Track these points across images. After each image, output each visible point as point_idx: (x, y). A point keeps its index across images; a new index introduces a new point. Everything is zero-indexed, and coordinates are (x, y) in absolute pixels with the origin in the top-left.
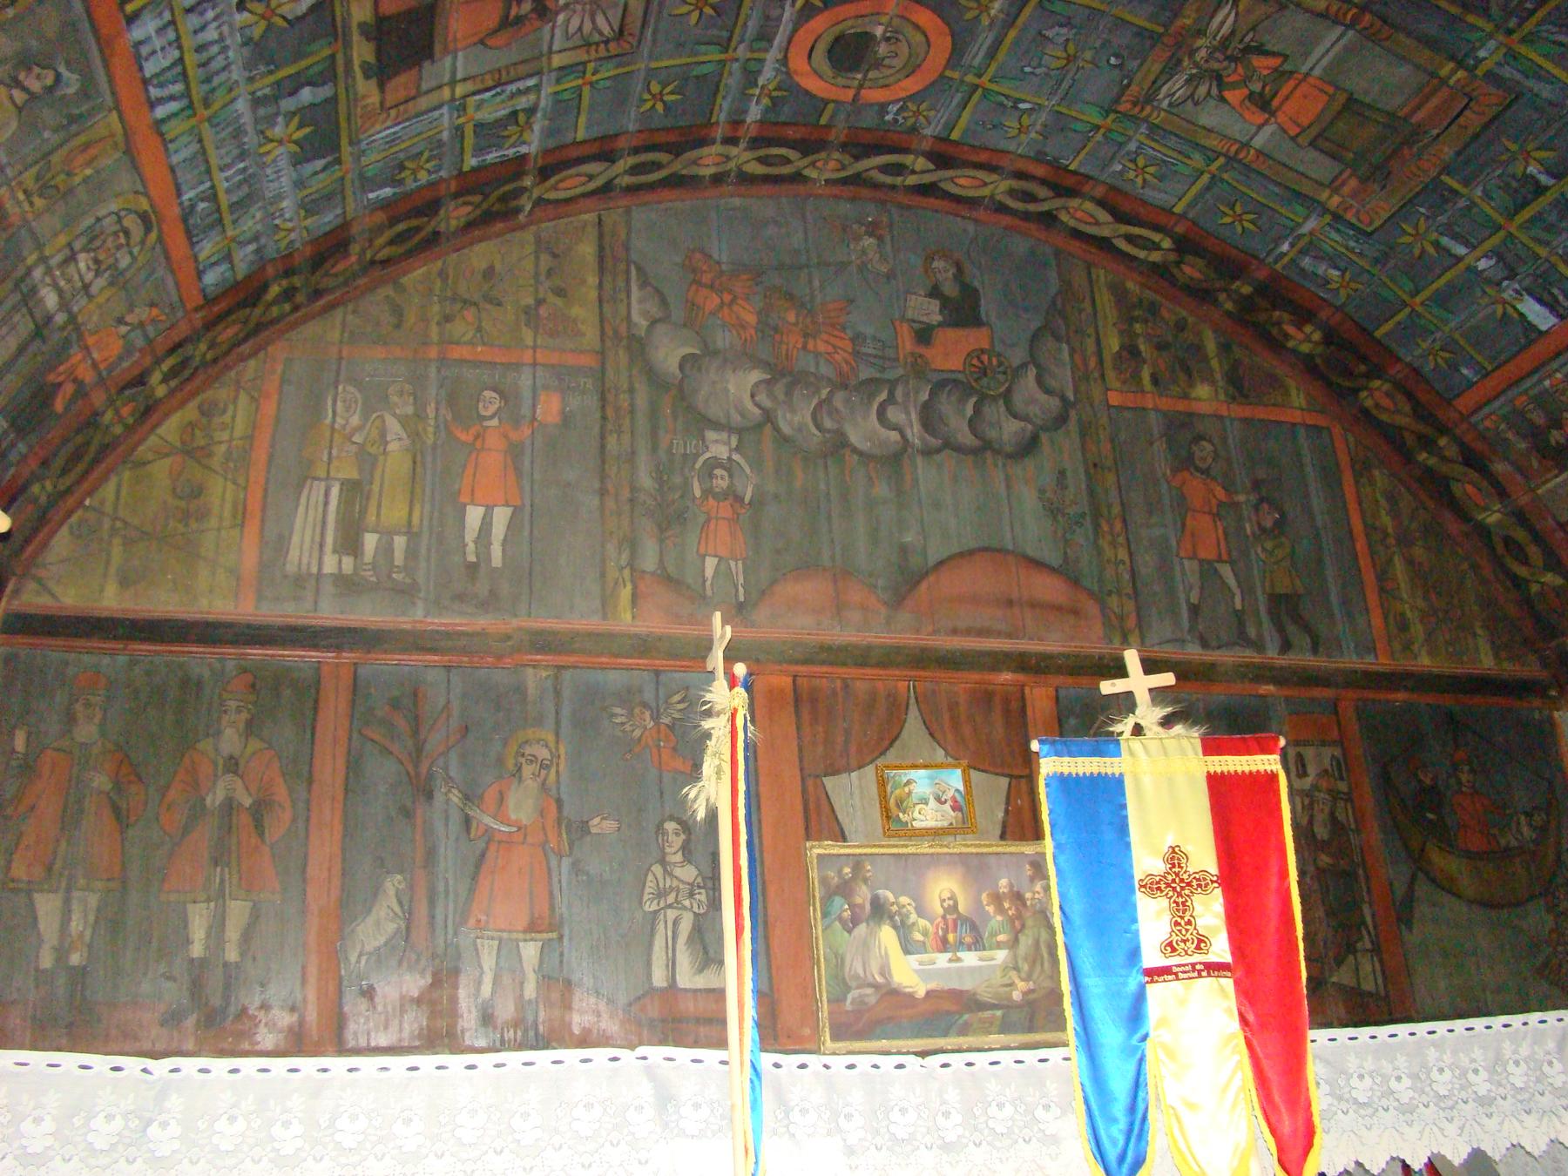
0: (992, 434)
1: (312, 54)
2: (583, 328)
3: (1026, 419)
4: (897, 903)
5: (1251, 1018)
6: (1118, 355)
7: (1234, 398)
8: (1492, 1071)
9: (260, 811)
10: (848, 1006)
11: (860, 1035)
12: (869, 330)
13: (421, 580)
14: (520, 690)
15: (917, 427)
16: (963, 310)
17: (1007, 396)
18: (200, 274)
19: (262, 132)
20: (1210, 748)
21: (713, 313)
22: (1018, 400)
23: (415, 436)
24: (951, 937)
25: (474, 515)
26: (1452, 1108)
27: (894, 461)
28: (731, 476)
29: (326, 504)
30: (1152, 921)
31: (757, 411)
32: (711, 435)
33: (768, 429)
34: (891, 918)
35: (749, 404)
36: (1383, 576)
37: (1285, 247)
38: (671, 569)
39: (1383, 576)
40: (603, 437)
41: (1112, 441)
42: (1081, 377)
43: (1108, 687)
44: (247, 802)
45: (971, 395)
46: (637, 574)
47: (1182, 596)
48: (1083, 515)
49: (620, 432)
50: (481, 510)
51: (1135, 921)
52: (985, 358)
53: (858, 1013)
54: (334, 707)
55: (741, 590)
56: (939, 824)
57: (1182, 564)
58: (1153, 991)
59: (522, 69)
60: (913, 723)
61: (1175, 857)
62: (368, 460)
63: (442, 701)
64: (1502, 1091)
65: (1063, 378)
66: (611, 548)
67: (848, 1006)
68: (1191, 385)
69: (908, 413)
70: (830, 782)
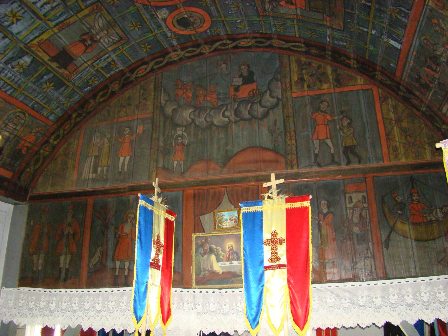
0: (255, 113)
1: (40, 70)
2: (149, 107)
3: (265, 107)
4: (216, 249)
5: (292, 281)
6: (297, 82)
7: (336, 86)
8: (414, 295)
9: (74, 235)
10: (201, 276)
11: (204, 284)
12: (221, 91)
13: (109, 178)
14: (129, 201)
15: (233, 115)
16: (248, 79)
17: (260, 102)
18: (48, 118)
19: (40, 88)
20: (288, 201)
21: (181, 96)
22: (263, 103)
23: (110, 142)
24: (231, 257)
25: (122, 159)
26: (396, 307)
27: (225, 127)
28: (182, 139)
29: (91, 162)
30: (267, 251)
31: (190, 120)
32: (178, 129)
33: (193, 124)
34: (214, 253)
35: (189, 119)
36: (388, 135)
37: (328, 40)
38: (166, 166)
39: (388, 135)
40: (152, 134)
41: (293, 108)
42: (284, 90)
43: (265, 185)
44: (72, 232)
45: (249, 104)
46: (157, 168)
47: (312, 152)
48: (282, 132)
49: (156, 132)
50: (123, 158)
51: (263, 253)
52: (254, 92)
53: (203, 278)
54: (90, 209)
55: (183, 169)
56: (230, 226)
57: (313, 142)
58: (268, 273)
59: (102, 53)
60: (225, 200)
61: (274, 234)
62: (100, 150)
63: (112, 206)
64: (417, 302)
65: (278, 93)
66: (152, 162)
67: (201, 276)
68: (321, 85)
69: (231, 112)
70: (201, 217)
